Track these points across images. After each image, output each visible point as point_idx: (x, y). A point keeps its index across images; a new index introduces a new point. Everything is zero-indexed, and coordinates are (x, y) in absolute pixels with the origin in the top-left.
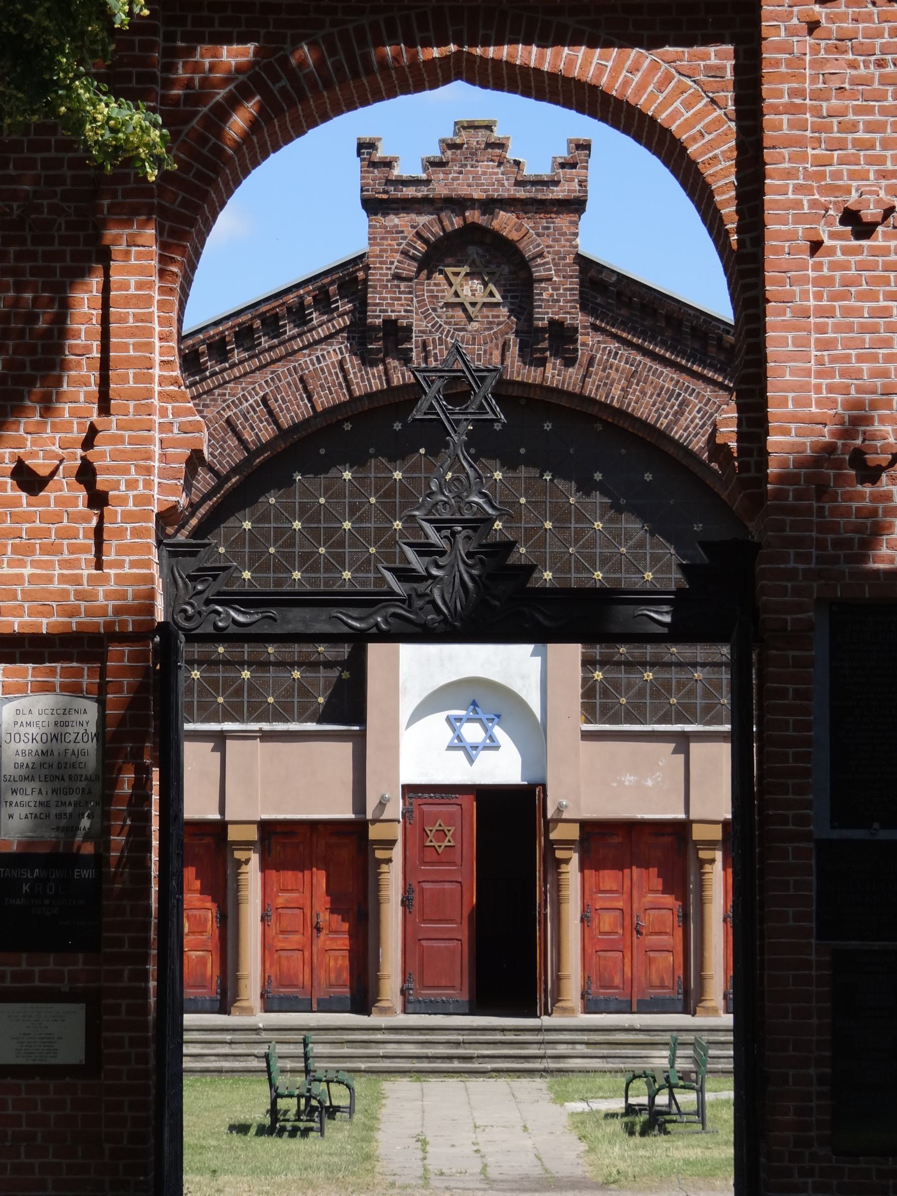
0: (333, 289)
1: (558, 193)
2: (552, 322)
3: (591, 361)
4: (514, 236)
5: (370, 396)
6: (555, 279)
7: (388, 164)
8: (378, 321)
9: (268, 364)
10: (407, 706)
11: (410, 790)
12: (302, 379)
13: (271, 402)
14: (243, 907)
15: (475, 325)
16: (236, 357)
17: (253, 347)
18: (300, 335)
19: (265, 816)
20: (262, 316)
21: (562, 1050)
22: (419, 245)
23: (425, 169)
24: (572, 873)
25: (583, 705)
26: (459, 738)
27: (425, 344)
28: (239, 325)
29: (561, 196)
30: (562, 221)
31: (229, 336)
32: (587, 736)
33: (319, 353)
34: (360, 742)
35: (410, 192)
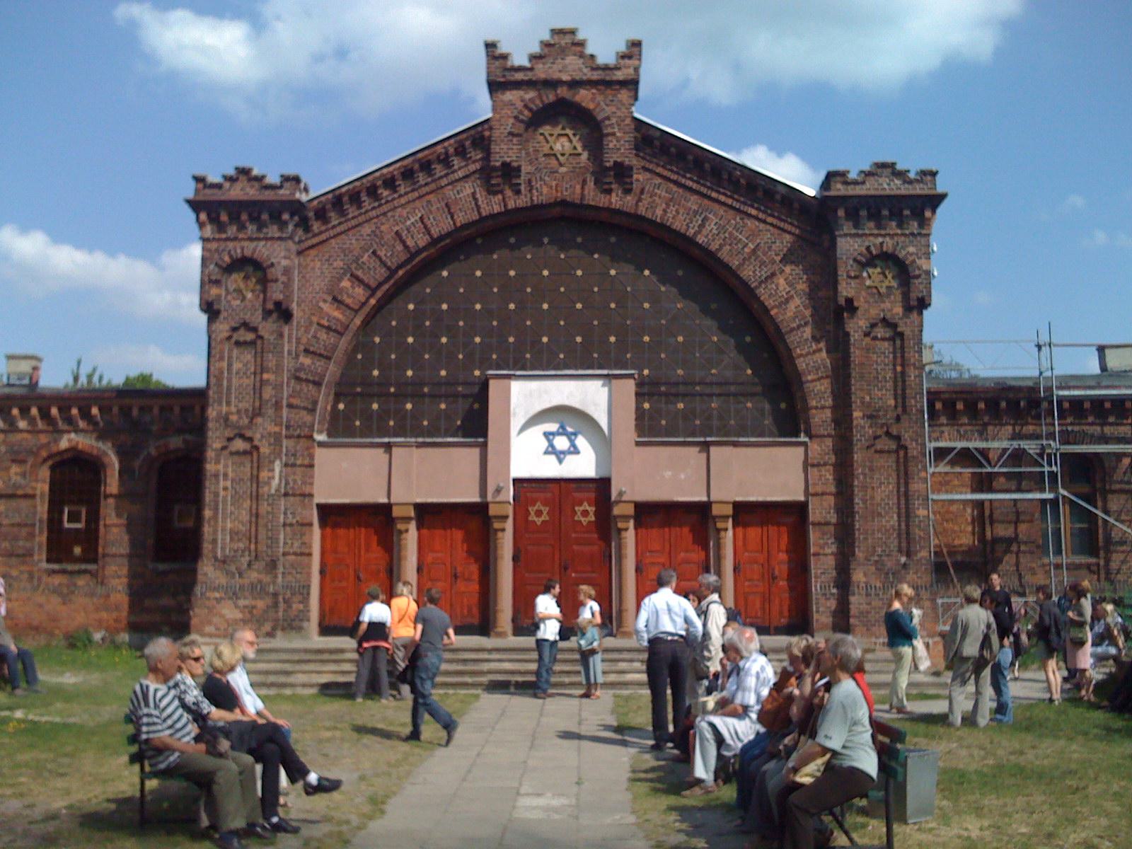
0: (468, 143)
1: (619, 75)
2: (615, 163)
3: (642, 192)
4: (591, 106)
5: (492, 216)
6: (618, 134)
7: (504, 57)
8: (498, 164)
9: (424, 196)
10: (516, 422)
11: (517, 481)
12: (447, 205)
13: (426, 220)
14: (403, 563)
15: (563, 170)
16: (402, 190)
17: (415, 183)
18: (446, 175)
19: (419, 500)
20: (419, 160)
21: (623, 666)
22: (526, 112)
23: (530, 60)
24: (630, 537)
25: (637, 426)
26: (551, 445)
27: (530, 181)
28: (405, 167)
29: (621, 78)
30: (624, 95)
31: (398, 176)
32: (638, 444)
33: (459, 188)
34: (484, 446)
35: (519, 76)
